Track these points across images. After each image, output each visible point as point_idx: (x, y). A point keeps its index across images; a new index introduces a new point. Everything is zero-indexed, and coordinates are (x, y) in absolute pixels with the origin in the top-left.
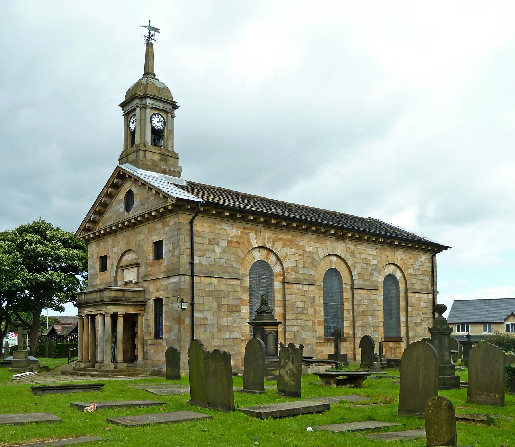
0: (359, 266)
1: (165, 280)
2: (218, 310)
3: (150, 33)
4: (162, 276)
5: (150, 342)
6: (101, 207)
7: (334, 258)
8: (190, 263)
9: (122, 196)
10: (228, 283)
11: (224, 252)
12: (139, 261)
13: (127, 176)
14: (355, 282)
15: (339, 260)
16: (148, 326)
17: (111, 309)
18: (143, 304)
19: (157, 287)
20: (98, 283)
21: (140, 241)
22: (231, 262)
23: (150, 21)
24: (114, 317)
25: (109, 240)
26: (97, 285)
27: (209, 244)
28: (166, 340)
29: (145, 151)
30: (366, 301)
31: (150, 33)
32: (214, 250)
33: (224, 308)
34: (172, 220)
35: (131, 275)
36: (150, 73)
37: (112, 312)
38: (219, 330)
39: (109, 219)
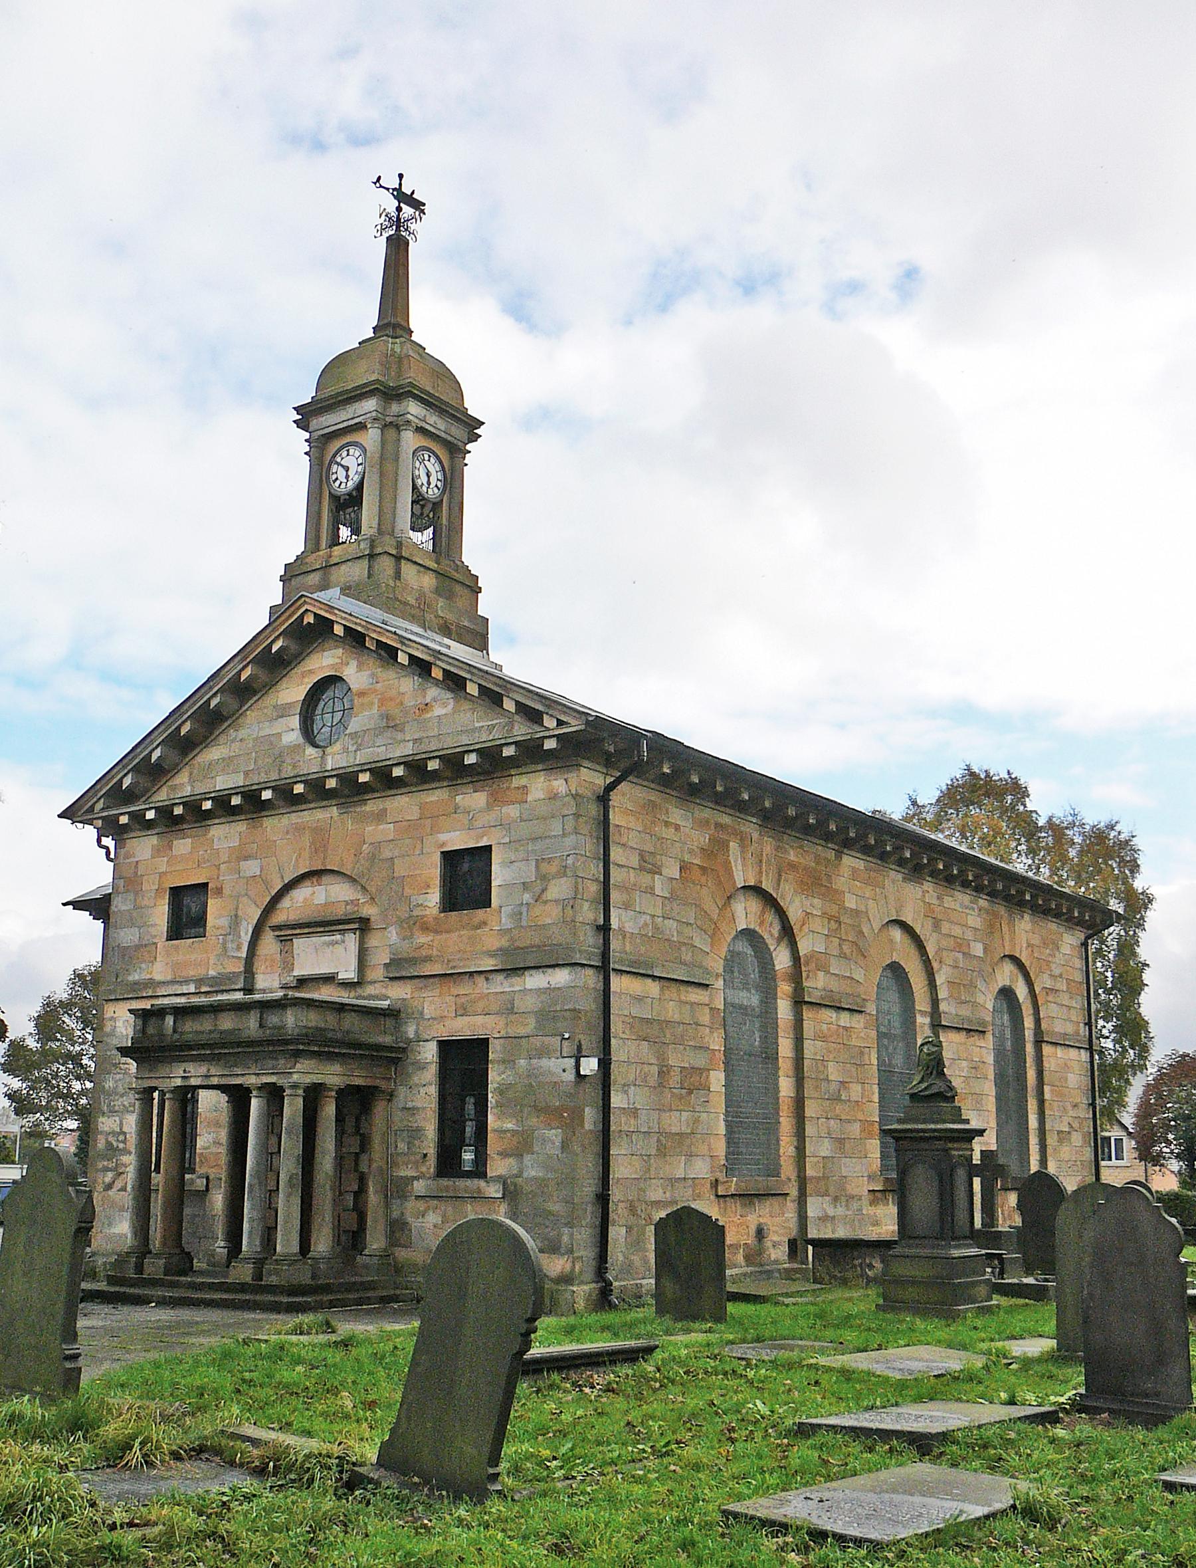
0: (949, 958)
1: (500, 977)
2: (661, 1085)
3: (399, 209)
4: (488, 964)
5: (419, 1187)
6: (203, 719)
7: (897, 934)
8: (598, 928)
9: (293, 691)
10: (683, 998)
11: (672, 897)
12: (369, 911)
13: (338, 630)
14: (943, 1007)
15: (907, 940)
16: (415, 1133)
17: (304, 1073)
18: (394, 1058)
19: (459, 1001)
20: (158, 977)
21: (377, 845)
22: (688, 931)
23: (401, 176)
24: (313, 1094)
25: (225, 835)
26: (152, 983)
27: (642, 869)
28: (503, 1180)
29: (398, 558)
30: (964, 1064)
31: (399, 209)
32: (650, 890)
33: (674, 1079)
34: (538, 785)
35: (333, 957)
36: (399, 326)
37: (308, 1080)
38: (662, 1152)
39: (221, 768)
